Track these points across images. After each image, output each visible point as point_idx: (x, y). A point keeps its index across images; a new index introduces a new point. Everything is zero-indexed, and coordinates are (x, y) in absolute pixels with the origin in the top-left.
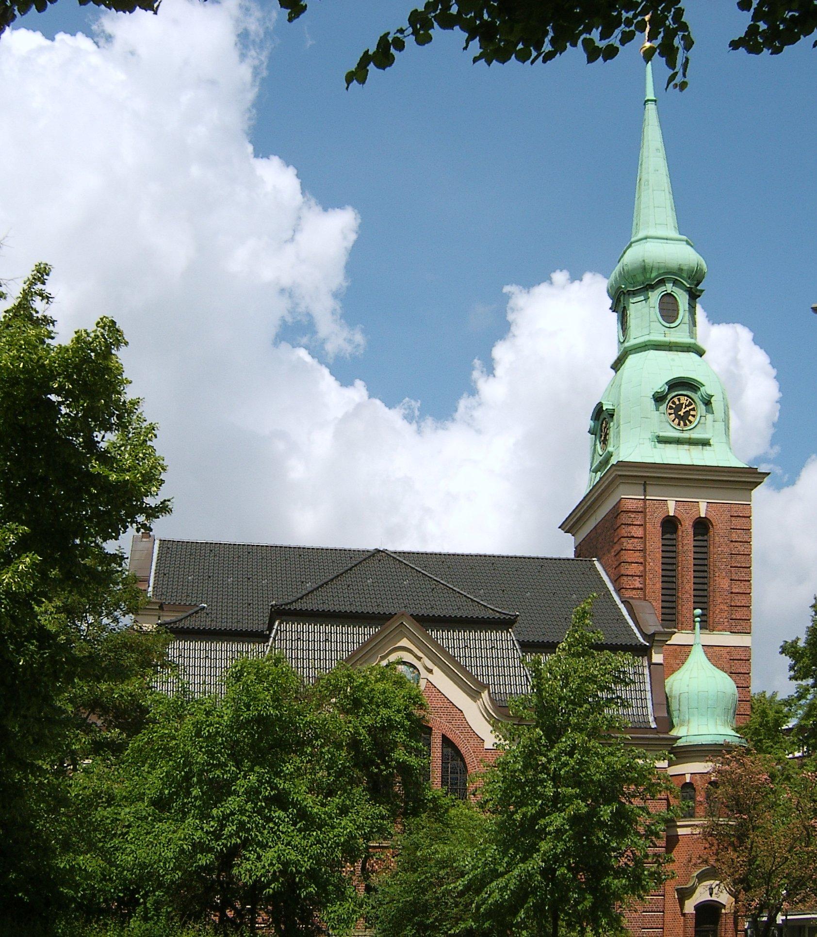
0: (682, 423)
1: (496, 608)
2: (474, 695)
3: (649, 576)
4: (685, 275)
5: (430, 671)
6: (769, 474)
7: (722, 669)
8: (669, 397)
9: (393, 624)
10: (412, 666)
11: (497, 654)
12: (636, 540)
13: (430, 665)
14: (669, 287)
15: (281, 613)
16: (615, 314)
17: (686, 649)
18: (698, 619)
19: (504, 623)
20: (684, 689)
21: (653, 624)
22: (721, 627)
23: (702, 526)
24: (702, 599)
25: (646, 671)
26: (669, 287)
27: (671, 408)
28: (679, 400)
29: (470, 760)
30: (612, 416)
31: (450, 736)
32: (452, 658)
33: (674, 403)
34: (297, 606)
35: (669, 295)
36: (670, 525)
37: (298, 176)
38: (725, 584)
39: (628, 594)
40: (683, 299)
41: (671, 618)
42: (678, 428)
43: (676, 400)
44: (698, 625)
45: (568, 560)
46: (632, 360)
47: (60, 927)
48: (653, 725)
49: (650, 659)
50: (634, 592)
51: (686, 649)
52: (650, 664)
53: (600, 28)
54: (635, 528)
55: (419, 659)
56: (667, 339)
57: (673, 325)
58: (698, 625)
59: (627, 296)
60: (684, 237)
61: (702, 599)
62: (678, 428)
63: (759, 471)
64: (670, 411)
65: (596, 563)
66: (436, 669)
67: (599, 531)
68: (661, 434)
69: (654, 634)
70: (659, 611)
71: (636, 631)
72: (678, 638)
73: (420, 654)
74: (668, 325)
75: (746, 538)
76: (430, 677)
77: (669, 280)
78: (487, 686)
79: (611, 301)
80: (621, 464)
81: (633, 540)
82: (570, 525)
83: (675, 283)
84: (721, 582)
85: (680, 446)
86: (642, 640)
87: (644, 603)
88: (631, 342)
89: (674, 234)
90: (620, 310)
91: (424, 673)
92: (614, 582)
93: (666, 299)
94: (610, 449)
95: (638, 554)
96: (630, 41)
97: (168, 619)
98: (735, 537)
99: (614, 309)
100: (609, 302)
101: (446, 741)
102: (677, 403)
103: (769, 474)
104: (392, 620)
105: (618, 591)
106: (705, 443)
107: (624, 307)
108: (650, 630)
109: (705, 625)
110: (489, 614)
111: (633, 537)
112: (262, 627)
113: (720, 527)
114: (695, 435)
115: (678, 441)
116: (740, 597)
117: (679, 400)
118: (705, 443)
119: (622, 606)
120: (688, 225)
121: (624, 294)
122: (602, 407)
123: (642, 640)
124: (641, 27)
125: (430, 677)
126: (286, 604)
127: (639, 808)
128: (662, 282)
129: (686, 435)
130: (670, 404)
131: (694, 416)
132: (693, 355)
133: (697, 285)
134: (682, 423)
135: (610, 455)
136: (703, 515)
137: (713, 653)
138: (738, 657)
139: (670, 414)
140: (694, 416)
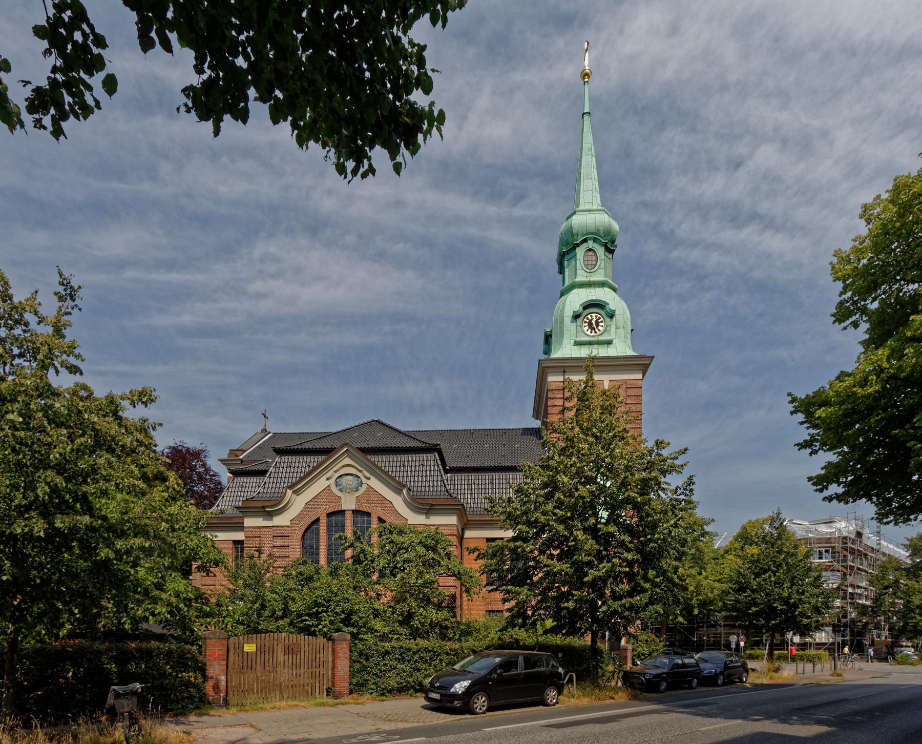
2: (399, 492)
5: (369, 479)
10: (357, 476)
14: (591, 244)
26: (591, 244)
35: (590, 250)
40: (600, 251)
53: (290, 118)
55: (361, 471)
63: (222, 124)
65: (588, 139)
66: (372, 478)
75: (638, 401)
76: (369, 482)
77: (590, 239)
83: (595, 240)
93: (590, 253)
96: (116, 85)
98: (629, 401)
106: (609, 343)
110: (420, 445)
118: (609, 343)
120: (607, 205)
125: (369, 482)
127: (504, 629)
128: (585, 241)
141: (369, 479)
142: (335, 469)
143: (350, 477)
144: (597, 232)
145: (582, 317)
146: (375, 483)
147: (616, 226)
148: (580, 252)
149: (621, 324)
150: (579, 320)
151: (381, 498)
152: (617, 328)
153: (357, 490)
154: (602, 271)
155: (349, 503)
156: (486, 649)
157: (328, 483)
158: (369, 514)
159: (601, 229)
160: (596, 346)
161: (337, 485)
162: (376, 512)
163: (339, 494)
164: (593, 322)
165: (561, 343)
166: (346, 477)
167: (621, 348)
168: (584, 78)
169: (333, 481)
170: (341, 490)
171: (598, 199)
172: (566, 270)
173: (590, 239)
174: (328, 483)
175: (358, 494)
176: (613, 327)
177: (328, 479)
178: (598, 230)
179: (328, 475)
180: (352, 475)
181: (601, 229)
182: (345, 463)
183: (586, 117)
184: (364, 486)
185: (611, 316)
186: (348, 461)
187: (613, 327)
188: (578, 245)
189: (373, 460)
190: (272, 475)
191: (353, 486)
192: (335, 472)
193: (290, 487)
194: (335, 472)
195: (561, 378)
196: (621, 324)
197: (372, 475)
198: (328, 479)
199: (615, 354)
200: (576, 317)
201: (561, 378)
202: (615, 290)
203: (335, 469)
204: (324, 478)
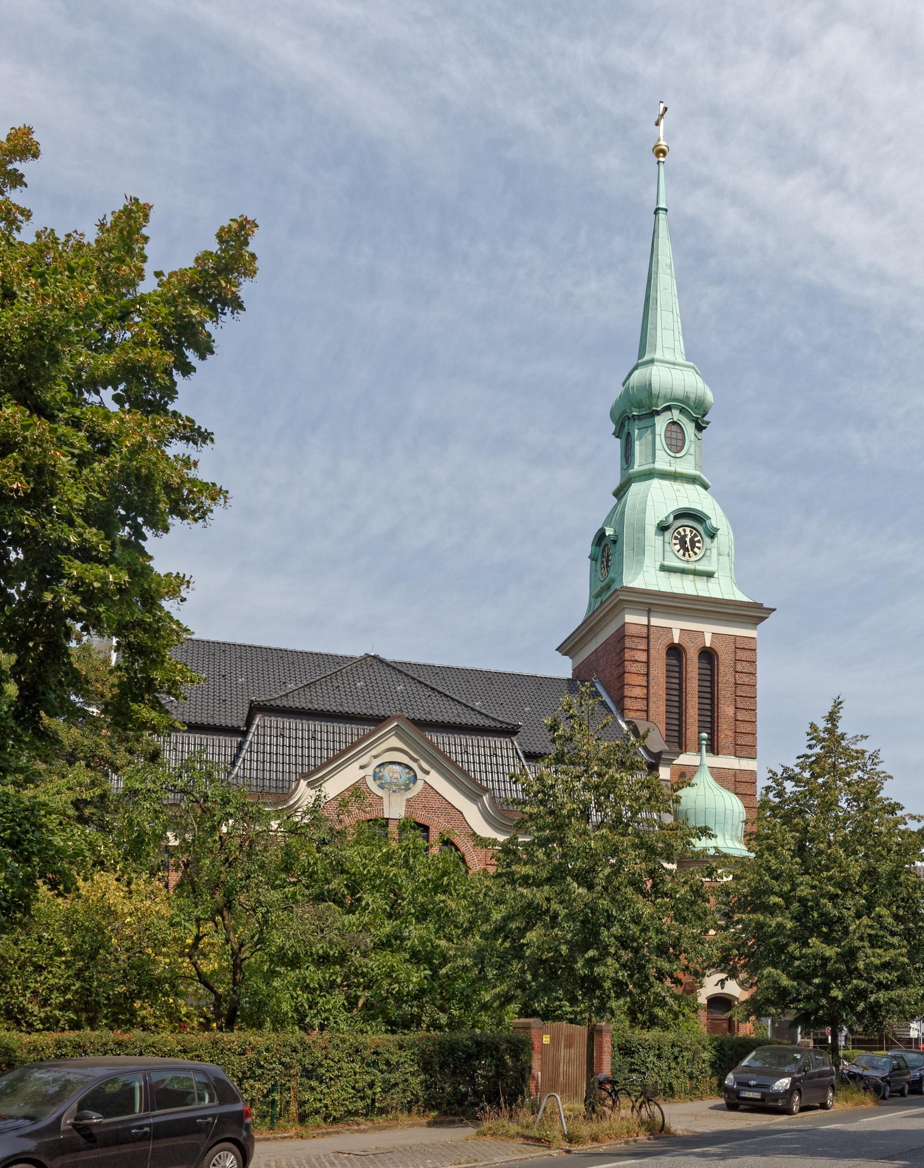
1: (507, 717)
3: (652, 699)
4: (692, 404)
5: (427, 773)
6: (774, 610)
7: (729, 790)
8: (674, 527)
11: (495, 760)
12: (640, 664)
13: (426, 766)
15: (255, 709)
16: (618, 440)
17: (695, 769)
18: (704, 742)
19: (509, 732)
20: (700, 802)
21: (656, 742)
22: (725, 751)
23: (708, 655)
26: (676, 415)
27: (676, 538)
28: (684, 531)
30: (615, 542)
32: (454, 764)
33: (679, 533)
34: (285, 703)
36: (675, 651)
41: (678, 740)
42: (683, 558)
43: (681, 530)
44: (704, 748)
46: (635, 488)
47: (914, 826)
50: (638, 713)
51: (695, 769)
54: (639, 652)
55: (415, 760)
56: (672, 469)
57: (678, 455)
58: (704, 748)
59: (632, 421)
60: (691, 364)
61: (710, 722)
62: (683, 558)
63: (765, 606)
64: (674, 541)
66: (433, 772)
67: (599, 654)
69: (660, 753)
70: (664, 733)
72: (685, 759)
73: (415, 756)
75: (751, 670)
77: (676, 407)
78: (486, 790)
79: (614, 426)
81: (637, 664)
82: (567, 648)
83: (682, 411)
84: (726, 710)
85: (685, 577)
88: (637, 467)
89: (681, 359)
90: (624, 436)
93: (674, 428)
94: (612, 575)
95: (641, 677)
99: (617, 434)
100: (612, 427)
102: (683, 534)
103: (774, 610)
106: (709, 575)
107: (629, 434)
109: (713, 749)
110: (487, 723)
111: (637, 661)
112: (241, 724)
113: (725, 658)
114: (700, 567)
115: (683, 571)
116: (747, 725)
117: (684, 531)
118: (709, 575)
120: (695, 356)
121: (629, 418)
122: (605, 533)
125: (428, 778)
128: (668, 408)
130: (676, 534)
131: (699, 548)
132: (698, 487)
133: (704, 416)
136: (708, 645)
137: (720, 776)
138: (744, 780)
139: (675, 544)
140: (699, 548)
141: (427, 773)
142: (374, 752)
143: (397, 768)
144: (685, 400)
145: (671, 530)
146: (436, 780)
147: (710, 397)
148: (661, 423)
149: (725, 550)
150: (668, 534)
151: (445, 805)
152: (719, 554)
153: (407, 789)
154: (691, 458)
155: (395, 809)
156: (356, 1113)
157: (362, 773)
158: (426, 829)
159: (692, 396)
160: (691, 577)
161: (375, 777)
162: (438, 826)
163: (380, 792)
164: (688, 540)
165: (640, 563)
166: (390, 766)
167: (723, 588)
168: (658, 156)
169: (369, 771)
170: (381, 786)
171: (680, 346)
172: (637, 443)
173: (676, 407)
174: (362, 773)
175: (409, 795)
176: (715, 551)
177: (362, 767)
178: (688, 398)
179: (364, 760)
180: (399, 764)
181: (692, 396)
182: (389, 745)
183: (662, 215)
184: (420, 784)
185: (712, 535)
186: (394, 742)
187: (715, 551)
188: (658, 413)
189: (434, 740)
190: (255, 747)
191: (401, 781)
192: (375, 757)
193: (305, 776)
194: (375, 757)
195: (643, 620)
196: (725, 550)
197: (433, 767)
198: (362, 767)
199: (719, 596)
200: (663, 528)
201: (643, 620)
202: (706, 487)
203: (374, 752)
204: (356, 765)
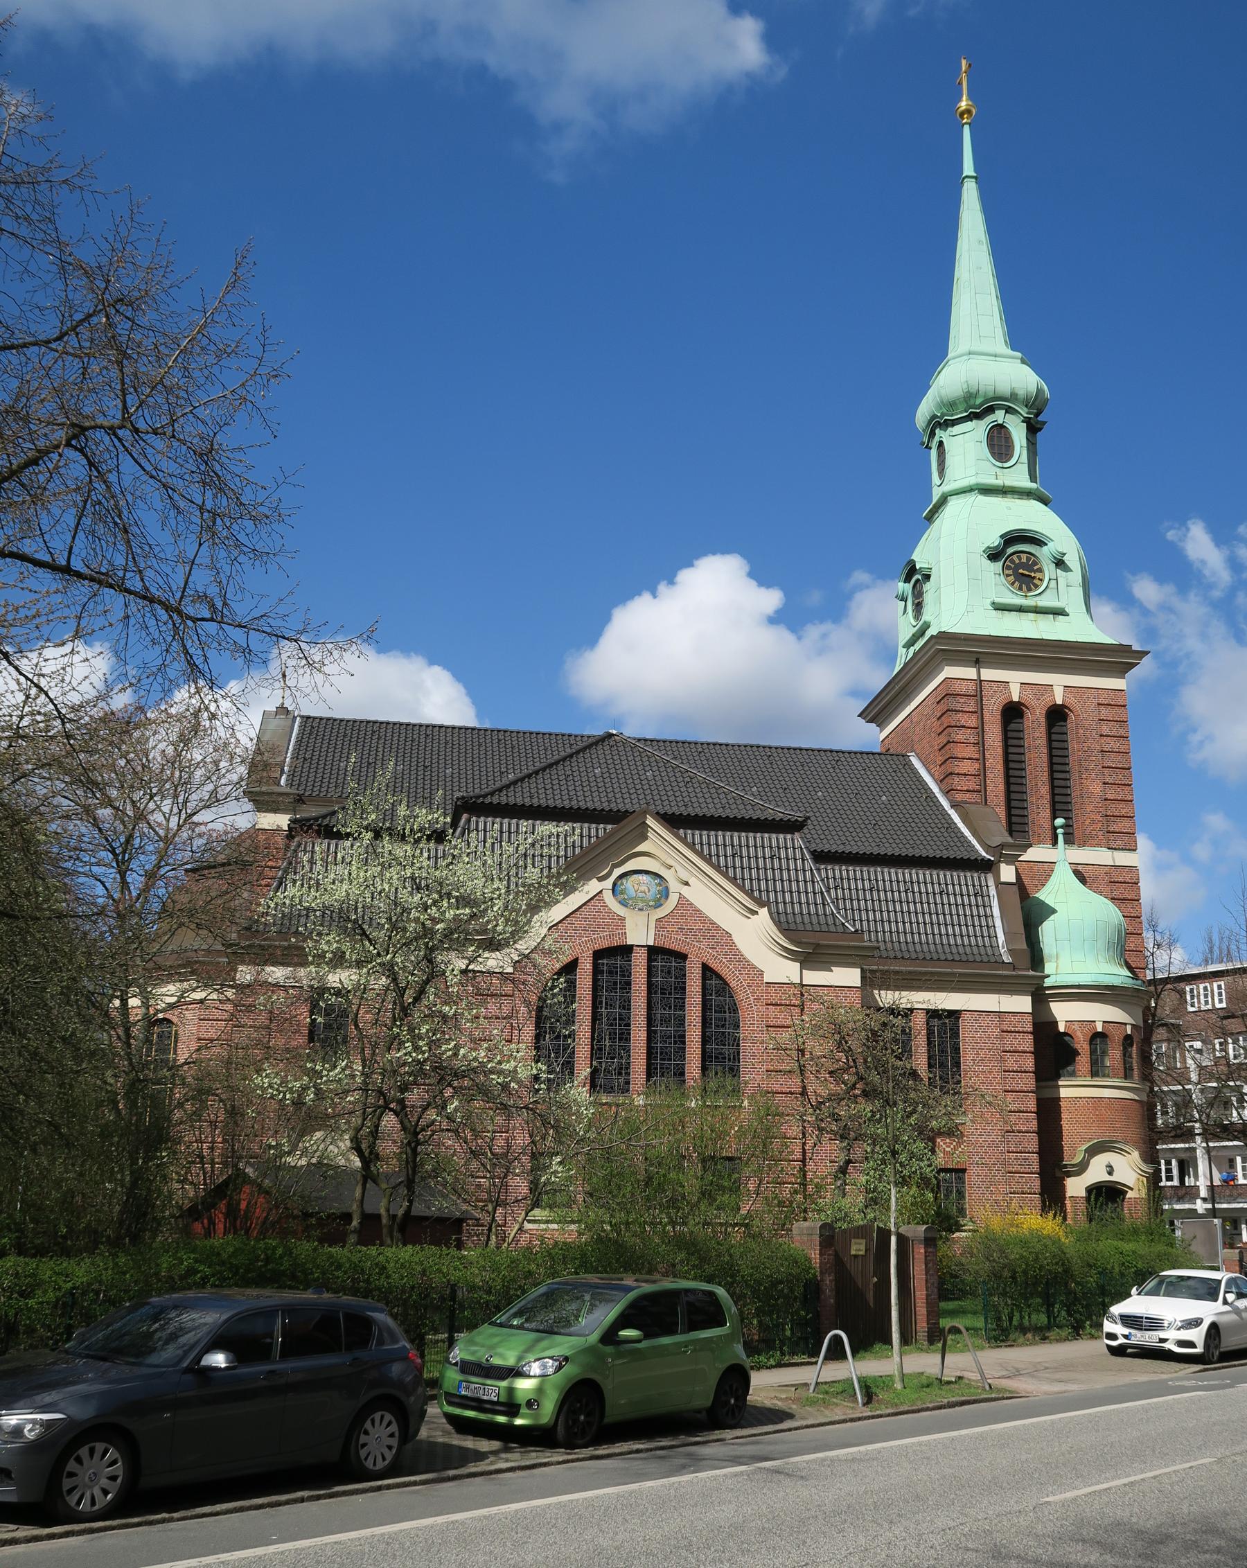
0: (1024, 587)
7: (1101, 893)
9: (629, 824)
14: (999, 416)
23: (1057, 715)
24: (1060, 803)
25: (993, 892)
27: (1009, 568)
28: (1019, 558)
29: (744, 996)
31: (714, 965)
33: (1013, 562)
35: (1001, 426)
36: (1013, 712)
37: (690, 564)
38: (1096, 788)
39: (960, 797)
41: (1017, 826)
43: (1014, 557)
44: (1061, 838)
45: (873, 754)
48: (1007, 958)
49: (997, 877)
52: (999, 884)
56: (999, 482)
58: (1061, 838)
61: (1060, 803)
64: (1007, 572)
68: (997, 600)
71: (974, 842)
74: (1000, 464)
76: (685, 891)
77: (1000, 407)
80: (943, 636)
86: (984, 854)
87: (981, 808)
91: (674, 886)
92: (940, 782)
94: (926, 617)
97: (305, 815)
101: (706, 970)
104: (626, 821)
105: (947, 793)
106: (1059, 612)
108: (996, 841)
111: (964, 727)
114: (1043, 602)
115: (1021, 609)
117: (1019, 558)
118: (1059, 612)
119: (952, 812)
120: (1022, 336)
123: (984, 854)
124: (743, 1277)
125: (685, 891)
126: (485, 796)
129: (1030, 602)
133: (1037, 415)
134: (1024, 587)
135: (927, 626)
139: (1008, 575)
